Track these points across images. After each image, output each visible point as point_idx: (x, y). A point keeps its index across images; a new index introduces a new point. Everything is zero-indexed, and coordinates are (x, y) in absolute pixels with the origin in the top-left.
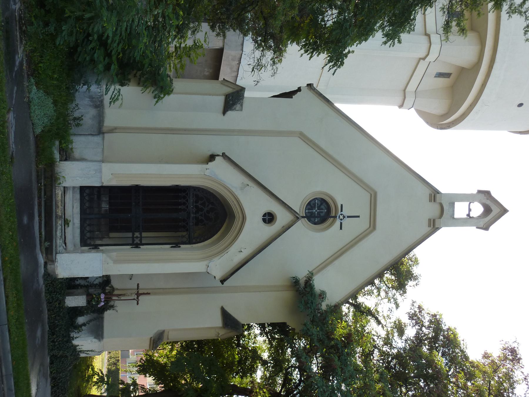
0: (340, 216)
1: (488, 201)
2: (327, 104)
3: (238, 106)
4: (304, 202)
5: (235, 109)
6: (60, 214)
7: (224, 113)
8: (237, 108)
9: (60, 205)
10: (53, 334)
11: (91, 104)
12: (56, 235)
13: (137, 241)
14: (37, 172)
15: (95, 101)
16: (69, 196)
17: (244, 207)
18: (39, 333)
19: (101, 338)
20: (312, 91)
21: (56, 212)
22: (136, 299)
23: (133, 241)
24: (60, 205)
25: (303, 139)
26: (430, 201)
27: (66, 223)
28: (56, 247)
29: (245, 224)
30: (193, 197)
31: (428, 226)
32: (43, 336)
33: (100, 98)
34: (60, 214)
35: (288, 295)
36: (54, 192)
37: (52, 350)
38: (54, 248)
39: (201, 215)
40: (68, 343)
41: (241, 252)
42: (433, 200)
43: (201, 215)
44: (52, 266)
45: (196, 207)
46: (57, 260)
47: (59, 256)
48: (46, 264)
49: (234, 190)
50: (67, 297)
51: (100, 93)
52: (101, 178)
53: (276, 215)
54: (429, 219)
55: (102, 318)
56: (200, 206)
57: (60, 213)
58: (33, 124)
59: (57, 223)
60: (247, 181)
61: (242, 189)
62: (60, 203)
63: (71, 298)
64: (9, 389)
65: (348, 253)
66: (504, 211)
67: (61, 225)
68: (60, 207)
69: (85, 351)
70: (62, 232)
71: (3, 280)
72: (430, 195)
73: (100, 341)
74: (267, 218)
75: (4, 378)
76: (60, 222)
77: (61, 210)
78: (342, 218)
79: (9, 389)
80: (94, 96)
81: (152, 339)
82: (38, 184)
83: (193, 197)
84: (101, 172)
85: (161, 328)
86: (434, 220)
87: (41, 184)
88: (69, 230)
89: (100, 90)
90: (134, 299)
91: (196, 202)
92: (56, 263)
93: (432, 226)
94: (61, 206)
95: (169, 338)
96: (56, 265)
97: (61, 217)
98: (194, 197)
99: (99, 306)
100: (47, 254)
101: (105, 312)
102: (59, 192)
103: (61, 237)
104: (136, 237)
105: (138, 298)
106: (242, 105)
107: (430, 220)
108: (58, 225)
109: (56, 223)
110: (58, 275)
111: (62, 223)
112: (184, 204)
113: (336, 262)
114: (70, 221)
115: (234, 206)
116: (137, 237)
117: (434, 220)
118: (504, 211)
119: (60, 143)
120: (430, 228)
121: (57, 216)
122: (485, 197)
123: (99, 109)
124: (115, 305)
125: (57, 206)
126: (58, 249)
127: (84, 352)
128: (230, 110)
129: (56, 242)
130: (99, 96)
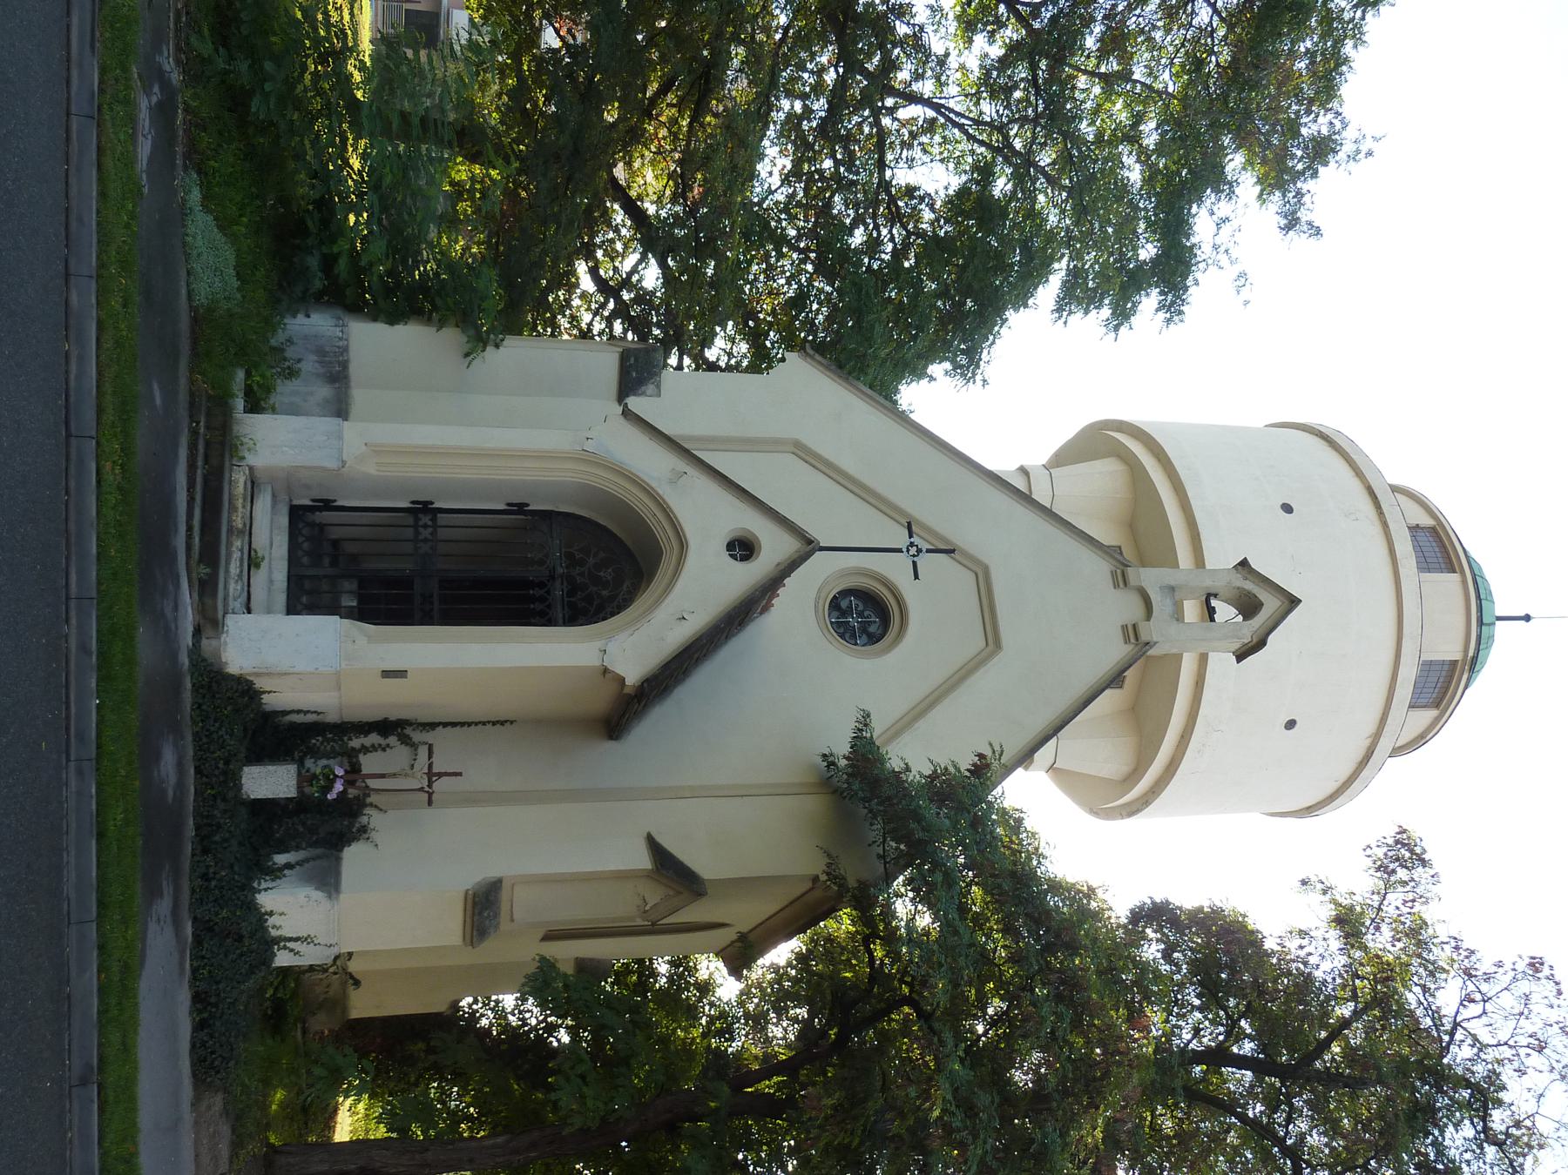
0: (911, 553)
1: (1248, 582)
2: (844, 384)
3: (650, 388)
4: (823, 595)
5: (644, 394)
6: (240, 526)
7: (651, 840)
8: (649, 392)
9: (240, 506)
10: (205, 851)
11: (322, 370)
12: (227, 571)
13: (425, 519)
14: (192, 394)
15: (330, 362)
16: (263, 504)
17: (681, 520)
18: (168, 758)
19: (332, 890)
20: (809, 360)
21: (230, 521)
22: (427, 789)
23: (417, 533)
24: (240, 506)
25: (803, 455)
26: (1116, 586)
27: (253, 562)
28: (225, 599)
29: (688, 558)
30: (562, 584)
31: (1112, 587)
32: (180, 765)
33: (342, 354)
34: (240, 526)
35: (814, 805)
36: (227, 475)
37: (201, 901)
38: (221, 586)
39: (582, 574)
40: (244, 890)
41: (684, 618)
42: (1121, 585)
43: (582, 574)
44: (214, 643)
45: (570, 556)
46: (226, 628)
47: (231, 621)
48: (198, 632)
49: (654, 484)
50: (246, 769)
51: (341, 339)
52: (341, 451)
53: (757, 538)
54: (1122, 626)
55: (338, 860)
56: (578, 556)
57: (239, 523)
58: (189, 273)
59: (232, 546)
60: (681, 464)
61: (672, 482)
62: (241, 501)
63: (258, 770)
64: (84, 649)
65: (946, 702)
66: (1294, 602)
67: (241, 550)
68: (240, 509)
69: (291, 939)
70: (241, 565)
71: (95, 306)
72: (1113, 574)
73: (330, 897)
74: (737, 552)
75: (73, 604)
76: (238, 543)
77: (243, 517)
78: (915, 548)
79: (84, 649)
80: (327, 349)
81: (470, 897)
82: (193, 421)
83: (562, 584)
84: (340, 437)
85: (493, 873)
86: (1134, 626)
87: (198, 423)
88: (259, 578)
89: (342, 331)
90: (422, 789)
91: (571, 593)
92: (225, 635)
93: (1133, 640)
94: (244, 507)
95: (515, 917)
96: (222, 639)
97: (241, 532)
98: (566, 607)
99: (329, 797)
100: (201, 595)
101: (346, 849)
102: (240, 479)
103: (240, 576)
104: (422, 541)
105: (430, 786)
106: (658, 387)
107: (1124, 628)
108: (234, 549)
109: (229, 544)
110: (226, 663)
111: (242, 546)
112: (542, 599)
113: (922, 725)
114: (263, 558)
115: (656, 524)
116: (425, 526)
117: (1134, 626)
118: (1294, 602)
119: (248, 374)
120: (1131, 647)
121: (230, 530)
122: (1239, 575)
123: (337, 385)
124: (371, 826)
125: (233, 508)
126: (232, 604)
127: (288, 944)
128: (635, 395)
129: (226, 588)
130: (339, 347)
